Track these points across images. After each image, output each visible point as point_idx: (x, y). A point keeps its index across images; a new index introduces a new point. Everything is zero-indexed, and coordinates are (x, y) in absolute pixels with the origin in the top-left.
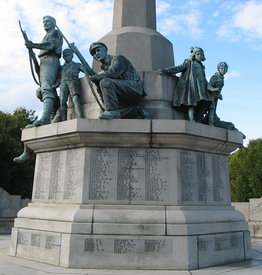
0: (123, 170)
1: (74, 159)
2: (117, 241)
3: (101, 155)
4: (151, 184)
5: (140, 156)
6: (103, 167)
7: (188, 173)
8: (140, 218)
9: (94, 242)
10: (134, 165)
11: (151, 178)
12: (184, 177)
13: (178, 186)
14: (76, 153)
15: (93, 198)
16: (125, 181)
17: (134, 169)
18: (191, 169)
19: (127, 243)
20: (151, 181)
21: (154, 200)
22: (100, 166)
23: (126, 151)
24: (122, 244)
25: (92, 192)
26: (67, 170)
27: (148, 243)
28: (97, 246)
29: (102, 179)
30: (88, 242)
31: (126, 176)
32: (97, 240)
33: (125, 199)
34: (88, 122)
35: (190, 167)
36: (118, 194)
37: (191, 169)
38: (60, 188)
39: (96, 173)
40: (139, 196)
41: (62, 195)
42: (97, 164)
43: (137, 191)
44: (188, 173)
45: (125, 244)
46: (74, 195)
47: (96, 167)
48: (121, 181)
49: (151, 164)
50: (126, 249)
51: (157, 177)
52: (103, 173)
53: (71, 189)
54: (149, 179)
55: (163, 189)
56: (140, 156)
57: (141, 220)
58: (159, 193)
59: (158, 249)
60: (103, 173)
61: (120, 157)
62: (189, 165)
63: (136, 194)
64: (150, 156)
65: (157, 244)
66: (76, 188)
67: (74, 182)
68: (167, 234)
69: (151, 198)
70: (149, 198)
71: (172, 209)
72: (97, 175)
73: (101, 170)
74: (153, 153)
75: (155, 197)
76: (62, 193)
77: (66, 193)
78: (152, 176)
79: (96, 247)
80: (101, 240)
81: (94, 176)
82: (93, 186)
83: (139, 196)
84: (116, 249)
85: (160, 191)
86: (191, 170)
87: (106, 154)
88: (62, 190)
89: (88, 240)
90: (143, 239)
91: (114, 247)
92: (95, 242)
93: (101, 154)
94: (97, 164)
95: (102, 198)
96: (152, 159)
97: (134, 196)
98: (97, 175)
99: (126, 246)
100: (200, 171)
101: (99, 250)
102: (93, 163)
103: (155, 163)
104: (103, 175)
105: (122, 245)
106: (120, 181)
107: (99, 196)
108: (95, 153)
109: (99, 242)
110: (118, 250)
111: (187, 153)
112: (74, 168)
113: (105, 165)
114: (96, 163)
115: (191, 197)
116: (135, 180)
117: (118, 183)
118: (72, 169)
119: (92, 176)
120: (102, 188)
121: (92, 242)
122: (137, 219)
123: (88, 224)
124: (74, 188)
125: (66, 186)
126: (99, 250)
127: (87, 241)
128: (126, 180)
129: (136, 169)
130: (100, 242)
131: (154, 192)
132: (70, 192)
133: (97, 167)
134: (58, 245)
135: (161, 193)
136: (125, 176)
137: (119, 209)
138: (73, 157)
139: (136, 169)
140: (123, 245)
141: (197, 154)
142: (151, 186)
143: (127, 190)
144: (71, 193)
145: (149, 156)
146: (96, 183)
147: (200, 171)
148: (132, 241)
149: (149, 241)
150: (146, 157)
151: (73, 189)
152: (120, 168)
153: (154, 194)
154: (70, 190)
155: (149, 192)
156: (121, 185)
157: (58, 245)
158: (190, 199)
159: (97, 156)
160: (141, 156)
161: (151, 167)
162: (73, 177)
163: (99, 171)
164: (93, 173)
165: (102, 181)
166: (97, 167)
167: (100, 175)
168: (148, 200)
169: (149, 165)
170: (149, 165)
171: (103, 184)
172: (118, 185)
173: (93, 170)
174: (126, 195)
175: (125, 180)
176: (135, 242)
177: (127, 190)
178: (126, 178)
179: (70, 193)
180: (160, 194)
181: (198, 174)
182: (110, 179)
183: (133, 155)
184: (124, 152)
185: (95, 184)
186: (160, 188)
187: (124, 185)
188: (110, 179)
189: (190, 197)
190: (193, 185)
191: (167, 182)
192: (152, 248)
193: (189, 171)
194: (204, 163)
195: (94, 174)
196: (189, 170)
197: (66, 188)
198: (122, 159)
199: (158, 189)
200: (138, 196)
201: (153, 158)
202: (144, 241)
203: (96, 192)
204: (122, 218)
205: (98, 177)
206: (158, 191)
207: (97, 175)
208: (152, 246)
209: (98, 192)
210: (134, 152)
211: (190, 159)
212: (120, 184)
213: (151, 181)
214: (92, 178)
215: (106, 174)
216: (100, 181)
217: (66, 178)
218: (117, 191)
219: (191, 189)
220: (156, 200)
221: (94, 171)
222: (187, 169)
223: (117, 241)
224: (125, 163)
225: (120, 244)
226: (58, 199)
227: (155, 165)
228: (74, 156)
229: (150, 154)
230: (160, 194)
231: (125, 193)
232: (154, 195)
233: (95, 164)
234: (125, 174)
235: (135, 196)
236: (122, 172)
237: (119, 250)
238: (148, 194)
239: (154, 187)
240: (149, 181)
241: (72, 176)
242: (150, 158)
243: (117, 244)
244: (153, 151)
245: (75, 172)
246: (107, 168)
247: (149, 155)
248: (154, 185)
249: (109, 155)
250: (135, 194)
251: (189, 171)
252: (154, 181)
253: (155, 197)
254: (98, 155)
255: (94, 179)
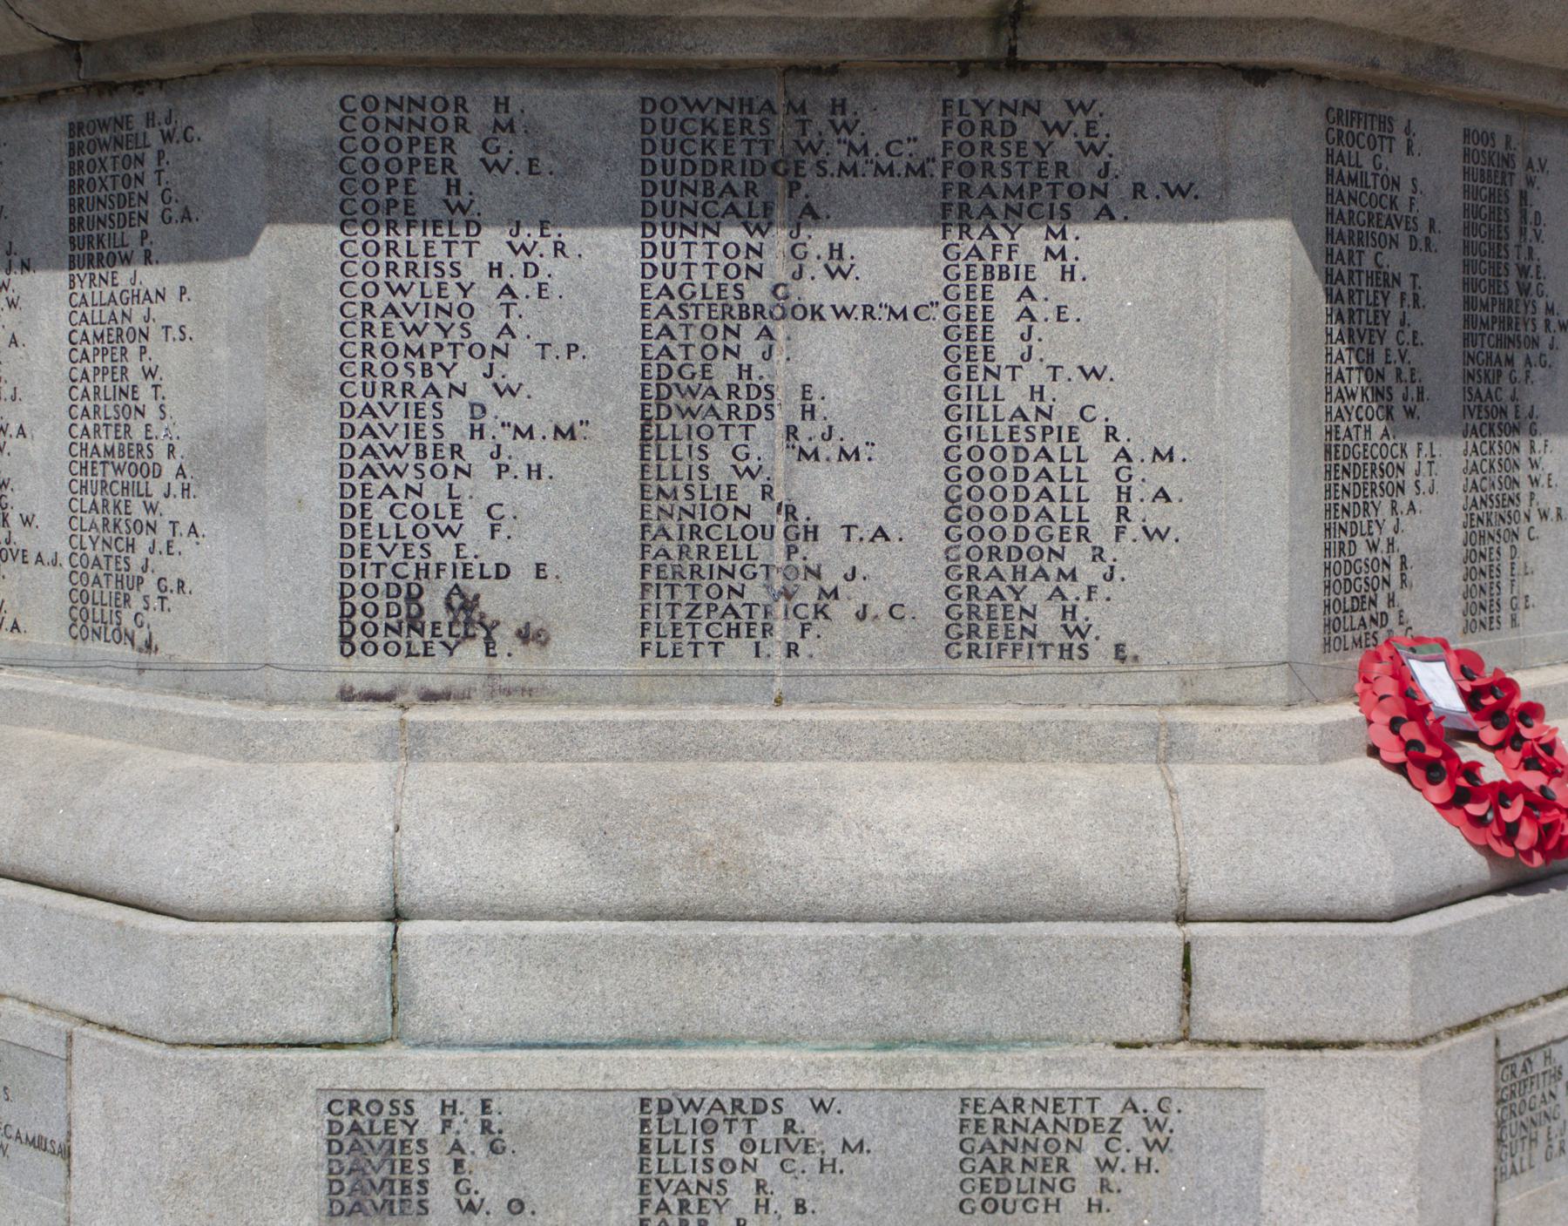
0: (694, 333)
1: (154, 208)
2: (665, 1108)
3: (448, 165)
4: (1009, 484)
5: (885, 163)
6: (481, 299)
7: (1390, 341)
8: (907, 857)
9: (419, 1132)
10: (814, 267)
11: (1006, 409)
12: (1353, 395)
13: (1293, 497)
14: (167, 137)
15: (380, 640)
16: (720, 455)
17: (816, 313)
18: (1416, 301)
19: (768, 1127)
20: (1008, 445)
21: (1037, 652)
22: (441, 287)
23: (724, 113)
24: (722, 1135)
25: (371, 570)
26: (90, 330)
27: (999, 1126)
28: (458, 1164)
29: (477, 432)
30: (355, 1128)
31: (733, 391)
32: (450, 1108)
33: (732, 646)
34: (1460, 629)
35: (1406, 283)
36: (651, 597)
37: (1416, 301)
38: (27, 522)
39: (400, 361)
40: (879, 607)
41: (52, 587)
42: (411, 269)
43: (851, 555)
44: (1390, 341)
45: (747, 1145)
46: (173, 598)
47: (397, 301)
48: (682, 451)
49: (1002, 258)
50: (760, 1186)
51: (1067, 398)
52: (480, 366)
53: (143, 541)
54: (987, 428)
55: (1134, 529)
56: (885, 163)
57: (912, 877)
58: (1091, 572)
59: (1104, 1186)
60: (480, 366)
61: (659, 177)
62: (1396, 260)
63: (842, 582)
64: (997, 161)
65: (1090, 1135)
66: (193, 530)
67: (169, 467)
68: (1197, 1033)
69: (1001, 633)
70: (983, 632)
71: (1232, 754)
72: (419, 393)
73: (456, 335)
74: (1029, 129)
75: (1049, 620)
76: (51, 570)
77: (92, 572)
78: (1014, 395)
79: (441, 1182)
80: (494, 1106)
81: (389, 402)
82: (379, 511)
83: (879, 607)
84: (653, 1187)
85: (1098, 554)
86: (1412, 315)
87: (512, 148)
88: (52, 536)
89: (354, 1107)
90: (949, 1082)
91: (635, 1176)
92: (428, 1121)
93: (448, 145)
94: (411, 269)
95: (482, 633)
96: (1013, 202)
97: (820, 611)
98: (421, 385)
99: (762, 1160)
100: (1484, 315)
101: (471, 1207)
102: (361, 155)
103: (1055, 245)
104: (480, 390)
105: (718, 1154)
106: (666, 452)
107: (443, 616)
108: (382, 135)
109: (468, 1129)
110: (674, 1206)
111: (1386, 122)
112: (156, 309)
113: (496, 269)
114: (402, 249)
115: (1403, 597)
116: (828, 436)
117: (653, 473)
118: (137, 322)
119: (360, 402)
120: (474, 526)
121: (402, 1132)
122: (878, 876)
123: (346, 944)
124: (174, 523)
125: (89, 499)
126: (471, 1207)
127: (347, 1121)
128: (736, 435)
129: (843, 313)
130: (486, 1128)
131: (1032, 569)
132: (136, 571)
133: (414, 297)
134: (38, 1143)
135: (1109, 577)
136: (722, 392)
137: (665, 753)
138: (141, 189)
139: (843, 313)
140: (727, 1145)
141: (1467, 135)
142: (1009, 504)
143: (742, 544)
144: (150, 580)
145: (988, 169)
146: (410, 478)
147: (1484, 315)
148: (820, 1107)
149: (1010, 1107)
150: (953, 176)
151: (164, 532)
152: (665, 327)
153: (1031, 585)
154: (131, 546)
155: (985, 567)
156: (682, 494)
157: (38, 1143)
158: (1393, 617)
159: (400, 177)
160: (900, 167)
161: (1006, 294)
162: (152, 414)
163: (436, 348)
164: (367, 369)
165: (475, 452)
166: (414, 297)
167: (444, 391)
168: (973, 652)
169: (979, 270)
170: (988, 271)
171: (483, 488)
172: (653, 493)
173: (367, 329)
174: (736, 601)
175: (720, 432)
176: (853, 1121)
177: (742, 544)
178: (733, 412)
179: (141, 580)
180: (1105, 589)
181: (1471, 350)
182: (565, 433)
183: (811, 160)
184: (706, 126)
185: (398, 484)
186: (1101, 513)
187: (709, 493)
188: (565, 433)
189: (1391, 600)
190: (1425, 469)
191: (1178, 455)
192: (1039, 1175)
193: (1394, 319)
194: (1522, 232)
195: (379, 380)
196: (1394, 306)
197: (93, 526)
198: (689, 200)
199: (1082, 534)
200: (861, 616)
201: (1035, 188)
202: (951, 1113)
203: (410, 570)
204: (713, 859)
205: (428, 411)
206: (1077, 555)
207: (421, 385)
208: (1030, 1156)
209: (440, 567)
210: (820, 121)
211: (1405, 192)
212: (667, 486)
213: (1008, 445)
214: (359, 427)
215: (511, 371)
216: (456, 450)
217: (78, 411)
218: (635, 564)
219: (1405, 520)
220: (1054, 653)
221: (378, 342)
222: (1380, 300)
223: (661, 1111)
224: (718, 250)
225: (701, 1137)
226: (15, 627)
227: (1055, 266)
228: (150, 179)
229: (997, 141)
230: (1105, 589)
231: (725, 582)
232: (1036, 592)
233: (382, 259)
234: (724, 372)
235: (834, 607)
236: (694, 353)
237: (684, 1206)
238: (973, 592)
239: (1034, 513)
240: (987, 447)
241: (145, 392)
242: (998, 184)
243: (668, 1142)
244: (1033, 108)
245: (169, 356)
246: (522, 306)
247: (987, 147)
248: (1035, 491)
249: (545, 161)
250: (829, 588)
251: (1394, 319)
252: (1034, 449)
253: (1049, 620)
254: (414, 163)
255: (383, 438)
